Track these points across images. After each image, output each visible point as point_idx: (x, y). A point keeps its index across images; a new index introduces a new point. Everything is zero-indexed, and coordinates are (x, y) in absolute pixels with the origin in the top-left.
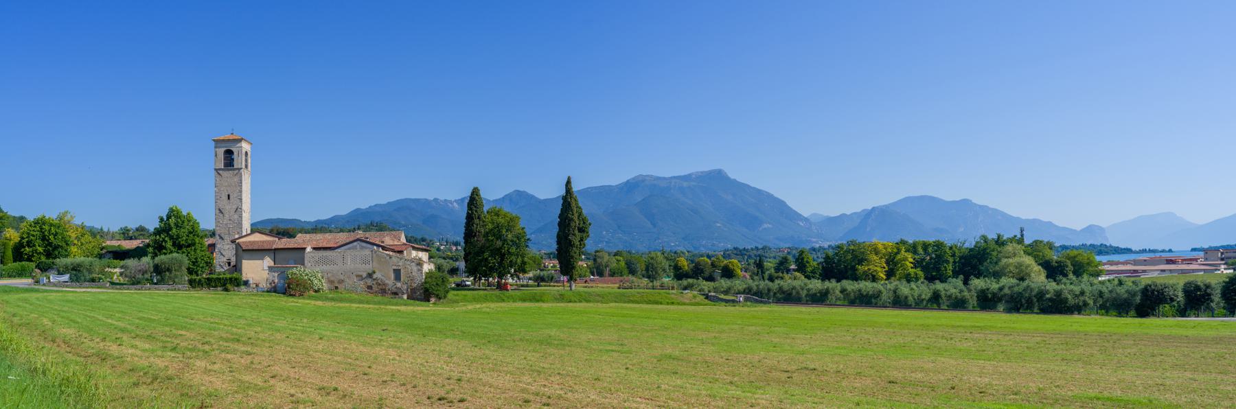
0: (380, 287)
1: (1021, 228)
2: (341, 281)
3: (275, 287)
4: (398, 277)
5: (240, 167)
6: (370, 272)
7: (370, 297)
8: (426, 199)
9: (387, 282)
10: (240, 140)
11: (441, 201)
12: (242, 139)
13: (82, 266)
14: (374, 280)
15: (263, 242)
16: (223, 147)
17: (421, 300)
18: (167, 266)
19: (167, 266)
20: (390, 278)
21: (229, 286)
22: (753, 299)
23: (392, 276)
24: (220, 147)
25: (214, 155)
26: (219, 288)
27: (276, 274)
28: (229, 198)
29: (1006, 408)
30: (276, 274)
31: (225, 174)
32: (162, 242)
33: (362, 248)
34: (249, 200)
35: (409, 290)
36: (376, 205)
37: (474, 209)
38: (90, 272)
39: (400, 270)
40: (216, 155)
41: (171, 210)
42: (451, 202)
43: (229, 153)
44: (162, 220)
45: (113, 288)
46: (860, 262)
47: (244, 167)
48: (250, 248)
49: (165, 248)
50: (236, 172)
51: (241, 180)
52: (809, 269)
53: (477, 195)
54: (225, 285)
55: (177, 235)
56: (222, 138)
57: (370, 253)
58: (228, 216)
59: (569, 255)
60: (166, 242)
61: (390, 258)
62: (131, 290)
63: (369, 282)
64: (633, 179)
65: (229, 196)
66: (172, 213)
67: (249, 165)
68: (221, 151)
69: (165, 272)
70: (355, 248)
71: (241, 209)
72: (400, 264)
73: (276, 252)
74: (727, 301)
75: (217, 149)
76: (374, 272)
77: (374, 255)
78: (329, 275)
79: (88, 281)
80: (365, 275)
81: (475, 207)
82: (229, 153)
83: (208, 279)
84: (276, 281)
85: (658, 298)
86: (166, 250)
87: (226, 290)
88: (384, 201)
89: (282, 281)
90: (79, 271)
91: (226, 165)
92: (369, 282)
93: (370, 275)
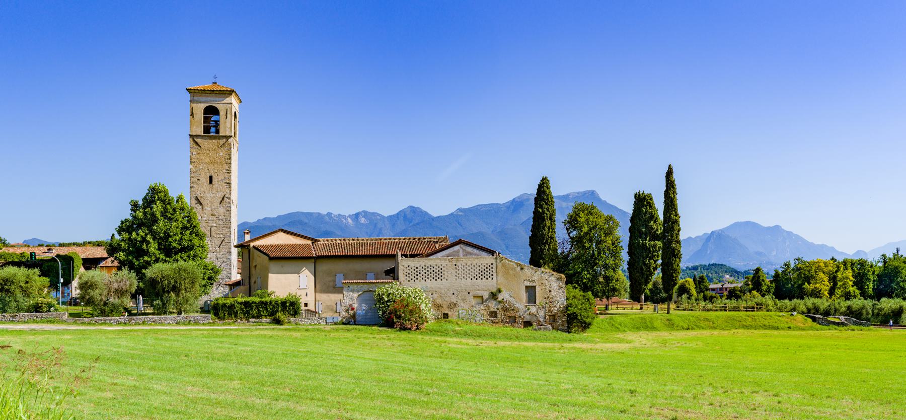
0: (508, 313)
1: (897, 248)
2: (452, 306)
3: (354, 316)
4: (532, 299)
5: (228, 134)
6: (494, 290)
7: (491, 329)
8: (319, 213)
9: (517, 305)
10: (231, 92)
11: (335, 216)
12: (233, 91)
13: (13, 282)
14: (500, 302)
15: (293, 246)
16: (203, 102)
17: (563, 331)
18: (173, 282)
19: (173, 282)
20: (521, 300)
21: (281, 315)
22: (853, 320)
23: (524, 295)
24: (197, 102)
25: (189, 113)
26: (264, 320)
27: (356, 295)
28: (211, 182)
29: (552, 415)
30: (356, 295)
31: (205, 143)
32: (142, 242)
33: (467, 254)
34: (237, 187)
35: (547, 317)
36: (265, 219)
37: (546, 206)
38: (26, 293)
39: (535, 287)
40: (192, 114)
41: (153, 191)
42: (344, 217)
43: (211, 111)
44: (135, 206)
45: (75, 322)
46: (808, 280)
47: (233, 135)
48: (288, 254)
49: (146, 253)
50: (222, 141)
51: (230, 155)
52: (764, 288)
53: (548, 188)
54: (273, 313)
55: (165, 233)
56: (201, 87)
57: (494, 262)
58: (209, 209)
59: (671, 269)
60: (148, 243)
61: (522, 269)
62: (111, 324)
63: (493, 305)
64: (519, 197)
65: (211, 178)
66: (154, 195)
67: (237, 133)
68: (200, 108)
69: (168, 292)
70: (456, 254)
71: (229, 198)
72: (535, 278)
73: (318, 261)
74: (838, 324)
75: (194, 105)
76: (500, 291)
77: (500, 265)
78: (435, 296)
79: (28, 311)
80: (486, 295)
81: (547, 204)
82: (211, 111)
83: (246, 304)
84: (355, 306)
85: (749, 322)
86: (150, 256)
87: (278, 322)
88: (274, 215)
89: (364, 307)
90: (8, 291)
91: (207, 130)
92: (493, 305)
93: (493, 296)
